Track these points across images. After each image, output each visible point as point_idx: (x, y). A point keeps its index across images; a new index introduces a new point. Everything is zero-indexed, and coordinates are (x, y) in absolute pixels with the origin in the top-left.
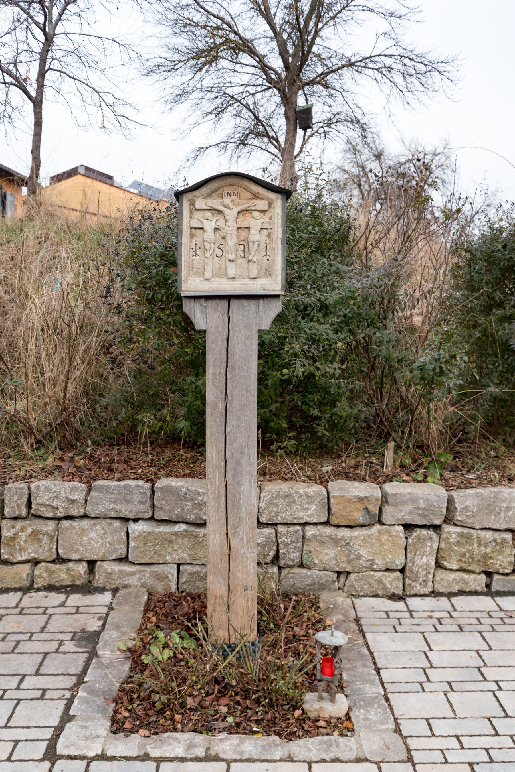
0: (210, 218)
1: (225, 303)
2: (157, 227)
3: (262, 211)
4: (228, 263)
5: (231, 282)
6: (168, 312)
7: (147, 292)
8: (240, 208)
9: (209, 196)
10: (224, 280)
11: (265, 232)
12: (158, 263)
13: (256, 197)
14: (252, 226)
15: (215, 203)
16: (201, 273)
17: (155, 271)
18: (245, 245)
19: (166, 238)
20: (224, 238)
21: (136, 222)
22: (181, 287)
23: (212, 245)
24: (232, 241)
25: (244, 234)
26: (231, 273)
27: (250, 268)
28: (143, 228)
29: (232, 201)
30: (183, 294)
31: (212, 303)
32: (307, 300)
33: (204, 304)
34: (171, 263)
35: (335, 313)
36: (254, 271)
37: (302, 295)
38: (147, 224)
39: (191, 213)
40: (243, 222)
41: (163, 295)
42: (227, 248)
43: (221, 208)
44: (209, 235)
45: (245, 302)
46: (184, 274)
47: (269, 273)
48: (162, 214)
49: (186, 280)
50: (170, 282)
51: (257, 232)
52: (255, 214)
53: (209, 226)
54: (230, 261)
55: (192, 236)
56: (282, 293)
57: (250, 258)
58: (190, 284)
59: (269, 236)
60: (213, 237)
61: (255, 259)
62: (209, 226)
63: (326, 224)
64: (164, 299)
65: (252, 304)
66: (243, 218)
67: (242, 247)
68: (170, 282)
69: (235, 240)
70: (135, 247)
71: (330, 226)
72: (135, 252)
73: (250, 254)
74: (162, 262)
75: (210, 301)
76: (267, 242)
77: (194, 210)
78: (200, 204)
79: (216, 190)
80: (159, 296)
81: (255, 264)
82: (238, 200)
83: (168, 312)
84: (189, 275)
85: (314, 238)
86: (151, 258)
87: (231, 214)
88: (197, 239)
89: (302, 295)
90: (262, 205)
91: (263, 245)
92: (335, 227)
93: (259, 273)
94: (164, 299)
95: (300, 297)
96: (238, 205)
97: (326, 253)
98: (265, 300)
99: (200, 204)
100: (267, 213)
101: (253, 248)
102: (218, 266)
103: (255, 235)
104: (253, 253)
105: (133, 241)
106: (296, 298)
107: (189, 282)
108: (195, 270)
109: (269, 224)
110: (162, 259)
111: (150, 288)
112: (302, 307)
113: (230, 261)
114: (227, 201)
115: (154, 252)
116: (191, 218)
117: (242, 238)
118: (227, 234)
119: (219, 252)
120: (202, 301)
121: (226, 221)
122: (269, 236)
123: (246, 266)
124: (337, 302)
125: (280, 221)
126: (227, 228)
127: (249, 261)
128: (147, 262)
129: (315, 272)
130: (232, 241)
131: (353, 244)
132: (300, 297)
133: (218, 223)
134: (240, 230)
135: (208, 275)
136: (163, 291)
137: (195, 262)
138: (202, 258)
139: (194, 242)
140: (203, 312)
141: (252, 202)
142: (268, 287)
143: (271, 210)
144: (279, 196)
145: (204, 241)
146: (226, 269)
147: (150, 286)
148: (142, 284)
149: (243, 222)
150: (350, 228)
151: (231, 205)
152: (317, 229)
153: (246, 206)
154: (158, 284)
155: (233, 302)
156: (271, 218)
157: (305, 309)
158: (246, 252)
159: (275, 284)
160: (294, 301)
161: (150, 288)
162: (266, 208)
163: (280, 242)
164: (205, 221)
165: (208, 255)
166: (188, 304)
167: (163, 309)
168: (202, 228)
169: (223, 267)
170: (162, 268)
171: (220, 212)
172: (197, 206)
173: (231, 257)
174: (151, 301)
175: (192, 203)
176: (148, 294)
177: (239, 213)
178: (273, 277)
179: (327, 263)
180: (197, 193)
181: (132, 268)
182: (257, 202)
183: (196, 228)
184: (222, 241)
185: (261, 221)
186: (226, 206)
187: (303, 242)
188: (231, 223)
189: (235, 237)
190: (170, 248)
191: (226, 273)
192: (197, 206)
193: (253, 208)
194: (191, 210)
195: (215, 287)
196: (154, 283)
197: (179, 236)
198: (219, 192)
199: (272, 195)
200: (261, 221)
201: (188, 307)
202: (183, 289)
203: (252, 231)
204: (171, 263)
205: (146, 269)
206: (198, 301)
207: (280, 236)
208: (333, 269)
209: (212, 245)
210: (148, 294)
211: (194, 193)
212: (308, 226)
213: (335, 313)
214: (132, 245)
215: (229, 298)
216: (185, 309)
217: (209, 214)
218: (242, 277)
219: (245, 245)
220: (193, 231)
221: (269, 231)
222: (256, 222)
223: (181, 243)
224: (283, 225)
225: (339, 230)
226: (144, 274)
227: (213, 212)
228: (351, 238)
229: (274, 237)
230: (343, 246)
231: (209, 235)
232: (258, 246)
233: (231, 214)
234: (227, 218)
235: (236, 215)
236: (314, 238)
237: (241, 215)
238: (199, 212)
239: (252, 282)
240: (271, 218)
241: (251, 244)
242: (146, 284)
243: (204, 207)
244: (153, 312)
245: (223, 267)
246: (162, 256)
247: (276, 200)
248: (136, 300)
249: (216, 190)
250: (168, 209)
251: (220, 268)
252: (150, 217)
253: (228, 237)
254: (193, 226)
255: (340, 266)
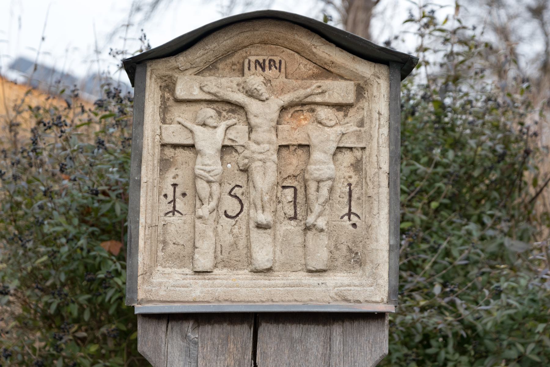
0: (210, 122)
1: (244, 332)
2: (76, 143)
3: (340, 107)
4: (255, 234)
5: (262, 280)
6: (93, 348)
7: (46, 299)
8: (286, 99)
9: (211, 67)
10: (243, 276)
11: (347, 158)
12: (73, 231)
13: (326, 71)
14: (314, 141)
15: (225, 85)
16: (186, 257)
17: (65, 250)
18: (298, 190)
19: (95, 169)
20: (245, 170)
21: (25, 135)
22: (135, 291)
23: (215, 187)
24: (264, 180)
25: (294, 162)
26: (262, 256)
27: (310, 243)
28: (41, 145)
29: (267, 81)
30: (139, 309)
31: (214, 333)
32: (435, 321)
33: (193, 335)
34: (103, 231)
35: (498, 353)
36: (320, 251)
37: (423, 309)
38: (51, 137)
39: (164, 109)
40: (292, 133)
41: (82, 309)
42: (253, 193)
43: (239, 97)
44: (209, 163)
45: (296, 331)
46: (142, 258)
47: (356, 259)
48: (85, 117)
49: (149, 273)
50: (101, 275)
51: (327, 158)
52: (323, 113)
53: (209, 140)
54: (259, 226)
55: (165, 164)
56: (391, 308)
57: (311, 220)
58: (160, 282)
59: (357, 166)
60: (218, 168)
61: (321, 223)
62: (209, 140)
63: (472, 143)
64: (86, 316)
65: (313, 337)
66: (294, 123)
67: (289, 193)
68: (101, 275)
69: (272, 177)
70: (19, 192)
71: (482, 146)
72: (18, 204)
73: (309, 210)
74: (84, 228)
75: (208, 328)
76: (353, 181)
77: (170, 100)
78: (187, 86)
79: (227, 54)
80: (74, 309)
81: (324, 239)
82: (282, 78)
83: (93, 348)
84: (155, 261)
85: (444, 176)
86: (58, 217)
87: (263, 112)
88: (180, 174)
89: (423, 309)
90: (340, 90)
91: (342, 189)
92: (493, 150)
93: (332, 259)
94: (86, 316)
95: (416, 315)
96: (282, 91)
97: (471, 211)
98: (347, 324)
99: (187, 86)
100: (352, 112)
101: (318, 197)
102: (229, 239)
103: (321, 165)
104: (317, 208)
105: (15, 178)
106: (409, 318)
107: (156, 279)
108: (171, 248)
109: (359, 137)
110: (83, 221)
111: (53, 290)
112: (418, 338)
113: (259, 226)
114: (255, 80)
115: (64, 205)
116: (164, 121)
117: (290, 170)
118: (252, 160)
119: (232, 206)
120: (188, 326)
121: (251, 130)
122: (357, 166)
123: (299, 239)
124: (500, 327)
125: (385, 131)
126: (254, 147)
127: (307, 229)
128: (47, 229)
129: (447, 253)
130: (264, 180)
131: (532, 191)
132: (416, 315)
133: (232, 134)
134: (285, 152)
135: (204, 261)
136: (83, 298)
137: (172, 229)
138: (189, 218)
139: (170, 181)
140: (188, 354)
141: (315, 83)
142: (354, 293)
143: (364, 103)
144: (382, 71)
145: (196, 177)
146: (248, 247)
147: (54, 286)
148: (33, 279)
149: (293, 132)
150: (527, 152)
151: (264, 92)
152: (451, 154)
153: (301, 93)
154: (72, 281)
155: (267, 331)
156: (361, 124)
157: (427, 340)
158: (300, 207)
159: (371, 287)
160: (402, 324)
161: (53, 290)
162: (351, 99)
163: (384, 181)
164: (198, 129)
165: (204, 211)
166: (151, 335)
167: (83, 340)
168: (192, 146)
169: (242, 243)
170: (82, 242)
171: (237, 108)
172: (181, 92)
173: (263, 218)
174: (53, 321)
175: (168, 86)
176: (48, 305)
177: (283, 109)
178: (368, 268)
179: (476, 234)
180: (181, 60)
181: (11, 241)
182: (327, 83)
183: (175, 146)
184: (241, 179)
185: (339, 129)
186: (251, 94)
187: (420, 185)
188: (264, 134)
189: (272, 167)
190: (104, 193)
191: (249, 257)
192: (181, 92)
193: (318, 99)
194: (164, 101)
195: (220, 292)
196: (63, 278)
197: (133, 165)
198: (235, 59)
199: (365, 69)
200: (339, 129)
201: (147, 340)
202: (141, 295)
203: (316, 155)
204: (103, 231)
205: (46, 243)
206: (176, 327)
207: (385, 167)
208: (492, 247)
209: (215, 187)
210: (48, 305)
211: (172, 61)
212: (431, 148)
213: (498, 353)
214: (12, 187)
215: (255, 320)
216: (145, 347)
217: (209, 112)
218: (288, 266)
219: (298, 190)
220: (169, 152)
221: (358, 154)
222: (325, 133)
223: (138, 183)
224: (391, 142)
225: (502, 157)
226: (38, 255)
227: (220, 106)
228: (528, 175)
229: (371, 170)
230: (510, 195)
231: (209, 163)
232: (331, 190)
233: (263, 112)
234: (254, 121)
235: (275, 116)
236: (444, 176)
237: (287, 116)
238: (184, 107)
239: (314, 280)
240: (361, 124)
241: (312, 186)
242: (46, 279)
243: (197, 94)
244: (58, 349)
245: (242, 243)
246: (84, 213)
247: (374, 81)
248: (17, 318)
249: (227, 54)
250: (100, 105)
251: (234, 245)
252: (59, 123)
253: (256, 166)
254: (168, 140)
255: (507, 241)
